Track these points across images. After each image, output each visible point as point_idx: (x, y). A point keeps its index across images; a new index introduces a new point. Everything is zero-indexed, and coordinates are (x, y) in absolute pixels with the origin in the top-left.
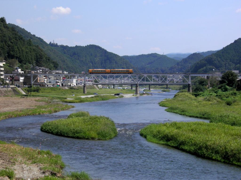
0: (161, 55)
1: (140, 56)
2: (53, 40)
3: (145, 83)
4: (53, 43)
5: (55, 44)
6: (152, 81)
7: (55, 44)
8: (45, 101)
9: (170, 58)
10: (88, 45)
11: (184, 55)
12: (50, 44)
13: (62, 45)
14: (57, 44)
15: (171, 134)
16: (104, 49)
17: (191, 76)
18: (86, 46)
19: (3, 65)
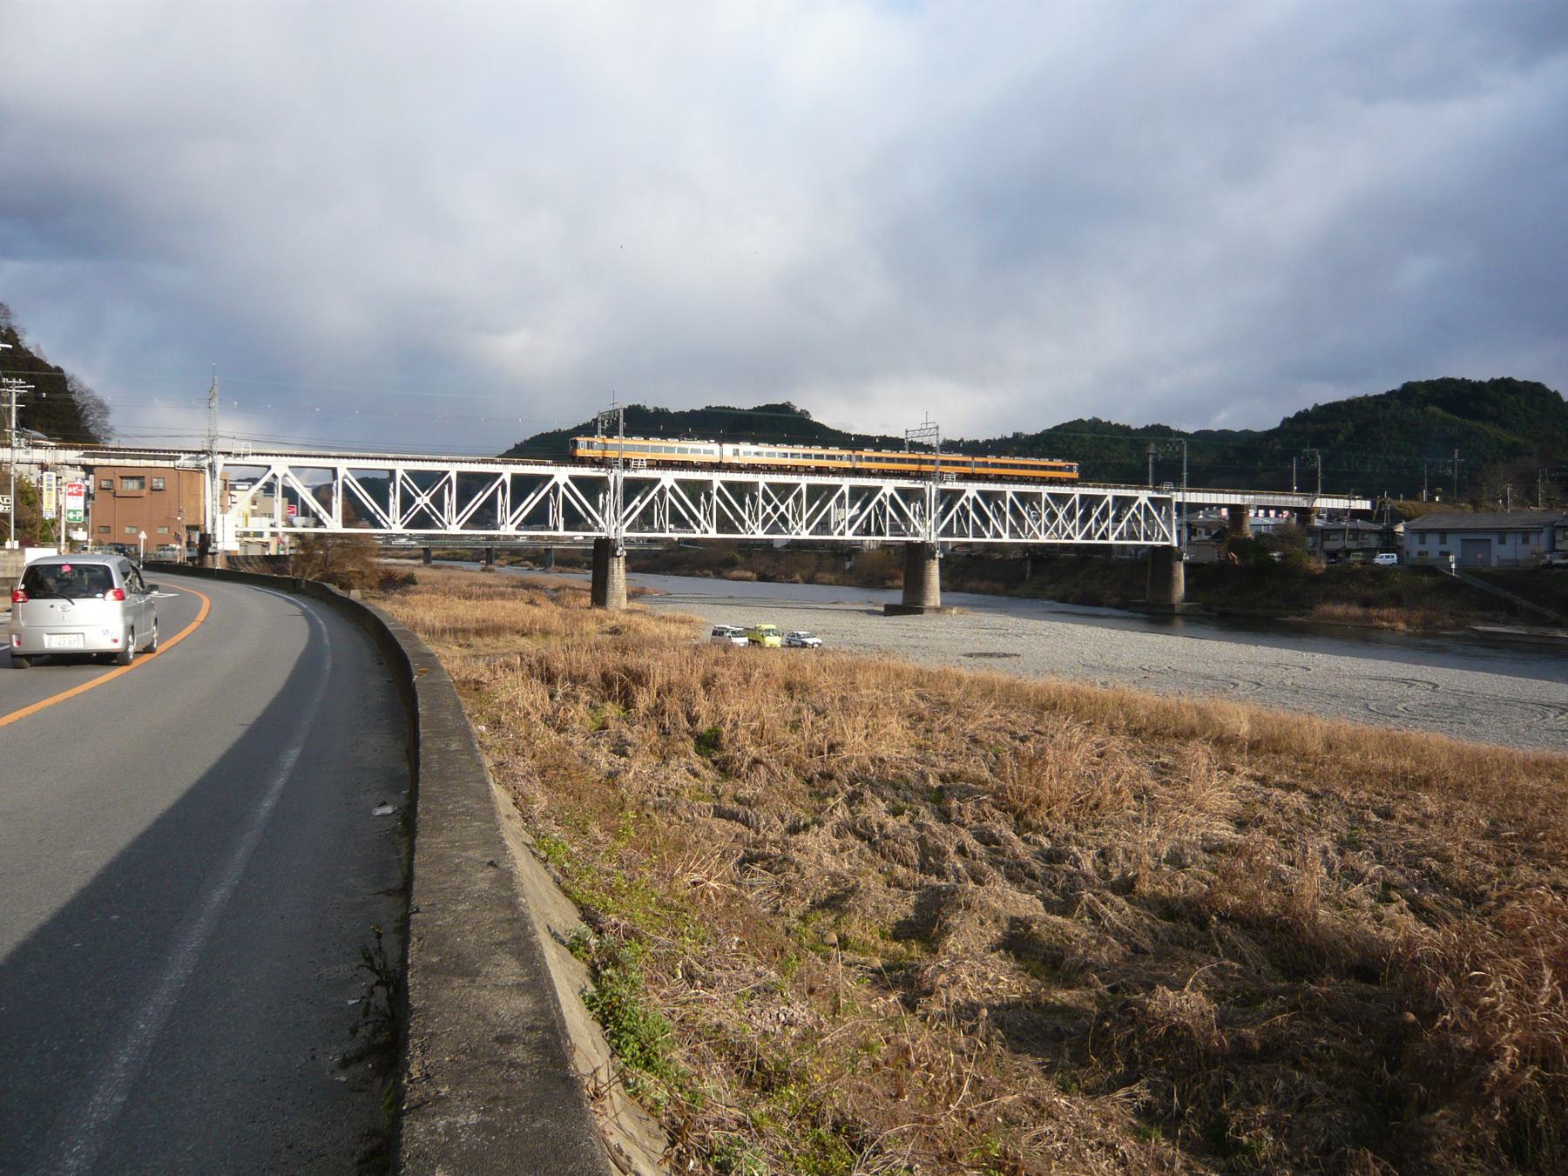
14: (516, 445)
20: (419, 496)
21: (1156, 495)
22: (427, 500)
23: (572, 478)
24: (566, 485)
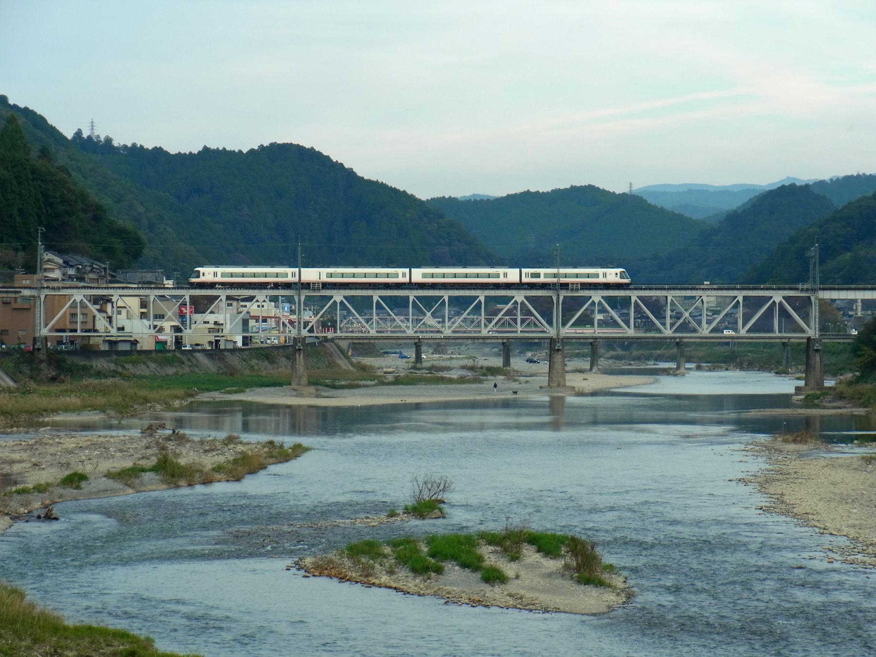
0: (563, 190)
1: (512, 199)
2: (92, 122)
3: (597, 331)
4: (89, 137)
5: (102, 138)
6: (629, 326)
7: (102, 138)
8: (241, 443)
9: (655, 207)
10: (262, 147)
11: (725, 193)
13: (134, 145)
14: (109, 141)
15: (611, 582)
16: (342, 164)
17: (820, 300)
18: (252, 151)
19: (199, 272)
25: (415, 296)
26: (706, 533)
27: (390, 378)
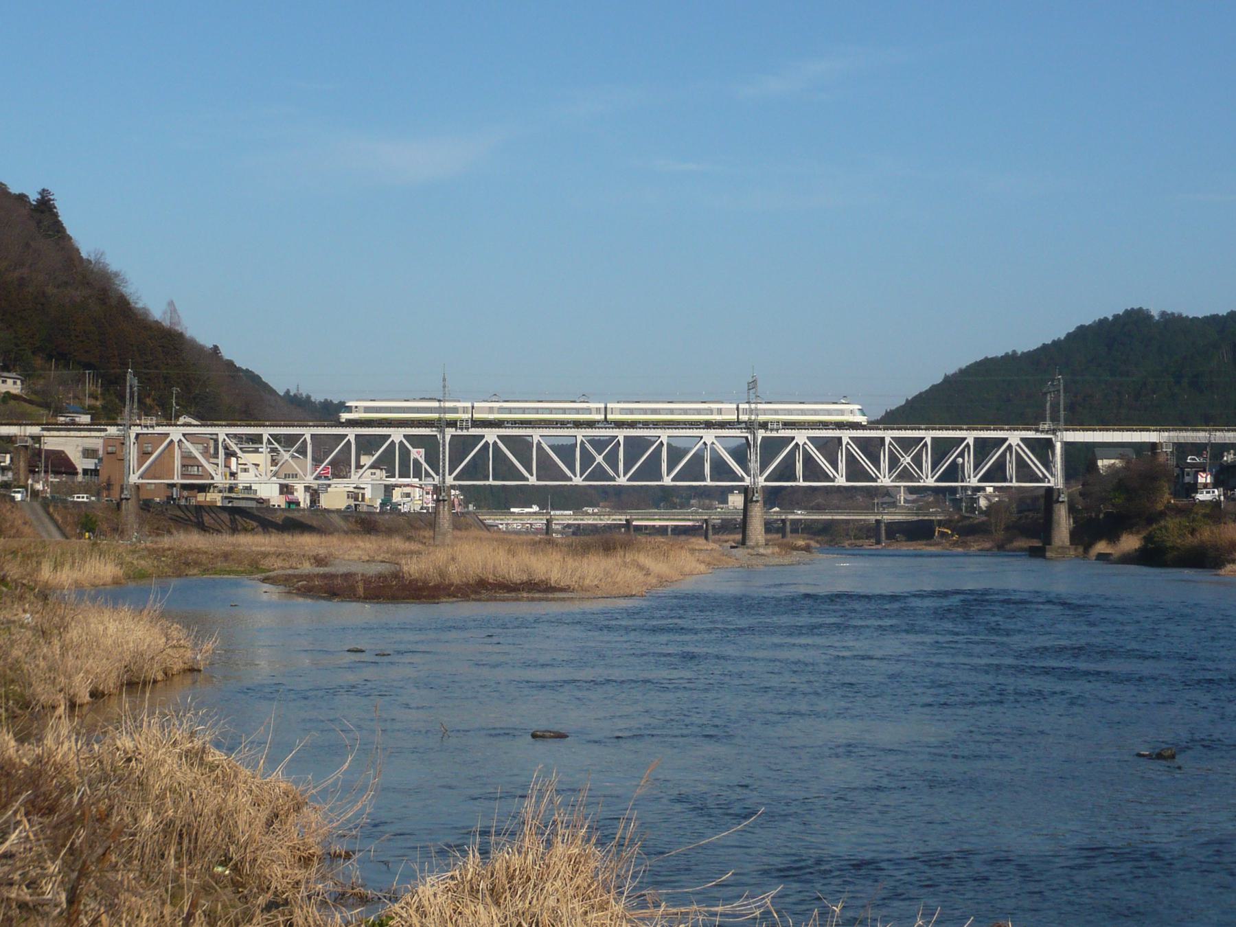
4: (295, 395)
5: (304, 396)
7: (304, 396)
10: (1132, 309)
12: (284, 395)
14: (308, 397)
20: (903, 457)
21: (1031, 434)
22: (908, 459)
23: (1023, 440)
24: (1018, 445)
25: (892, 438)
26: (101, 394)
27: (854, 598)
